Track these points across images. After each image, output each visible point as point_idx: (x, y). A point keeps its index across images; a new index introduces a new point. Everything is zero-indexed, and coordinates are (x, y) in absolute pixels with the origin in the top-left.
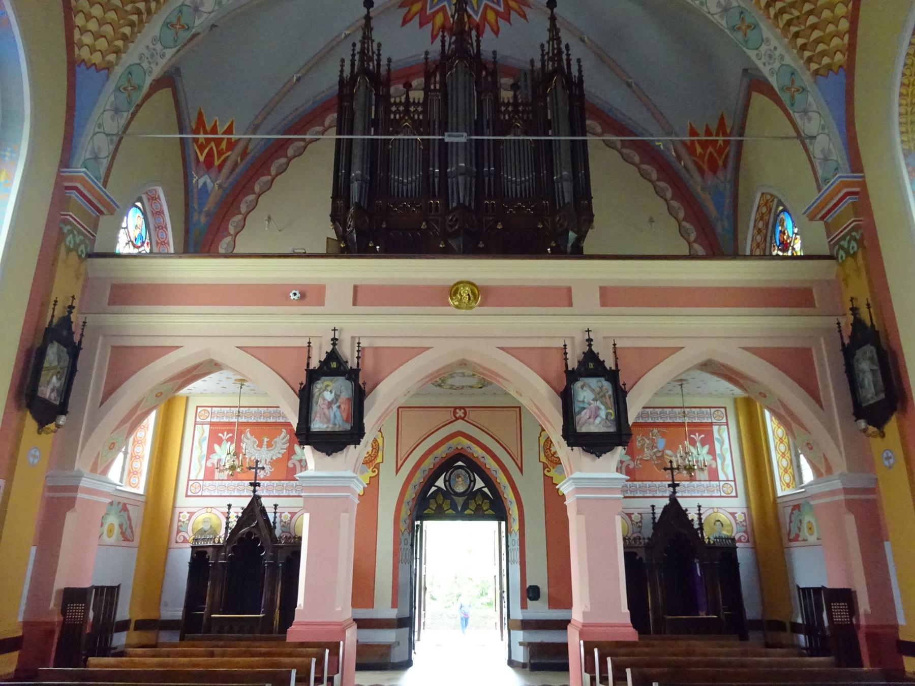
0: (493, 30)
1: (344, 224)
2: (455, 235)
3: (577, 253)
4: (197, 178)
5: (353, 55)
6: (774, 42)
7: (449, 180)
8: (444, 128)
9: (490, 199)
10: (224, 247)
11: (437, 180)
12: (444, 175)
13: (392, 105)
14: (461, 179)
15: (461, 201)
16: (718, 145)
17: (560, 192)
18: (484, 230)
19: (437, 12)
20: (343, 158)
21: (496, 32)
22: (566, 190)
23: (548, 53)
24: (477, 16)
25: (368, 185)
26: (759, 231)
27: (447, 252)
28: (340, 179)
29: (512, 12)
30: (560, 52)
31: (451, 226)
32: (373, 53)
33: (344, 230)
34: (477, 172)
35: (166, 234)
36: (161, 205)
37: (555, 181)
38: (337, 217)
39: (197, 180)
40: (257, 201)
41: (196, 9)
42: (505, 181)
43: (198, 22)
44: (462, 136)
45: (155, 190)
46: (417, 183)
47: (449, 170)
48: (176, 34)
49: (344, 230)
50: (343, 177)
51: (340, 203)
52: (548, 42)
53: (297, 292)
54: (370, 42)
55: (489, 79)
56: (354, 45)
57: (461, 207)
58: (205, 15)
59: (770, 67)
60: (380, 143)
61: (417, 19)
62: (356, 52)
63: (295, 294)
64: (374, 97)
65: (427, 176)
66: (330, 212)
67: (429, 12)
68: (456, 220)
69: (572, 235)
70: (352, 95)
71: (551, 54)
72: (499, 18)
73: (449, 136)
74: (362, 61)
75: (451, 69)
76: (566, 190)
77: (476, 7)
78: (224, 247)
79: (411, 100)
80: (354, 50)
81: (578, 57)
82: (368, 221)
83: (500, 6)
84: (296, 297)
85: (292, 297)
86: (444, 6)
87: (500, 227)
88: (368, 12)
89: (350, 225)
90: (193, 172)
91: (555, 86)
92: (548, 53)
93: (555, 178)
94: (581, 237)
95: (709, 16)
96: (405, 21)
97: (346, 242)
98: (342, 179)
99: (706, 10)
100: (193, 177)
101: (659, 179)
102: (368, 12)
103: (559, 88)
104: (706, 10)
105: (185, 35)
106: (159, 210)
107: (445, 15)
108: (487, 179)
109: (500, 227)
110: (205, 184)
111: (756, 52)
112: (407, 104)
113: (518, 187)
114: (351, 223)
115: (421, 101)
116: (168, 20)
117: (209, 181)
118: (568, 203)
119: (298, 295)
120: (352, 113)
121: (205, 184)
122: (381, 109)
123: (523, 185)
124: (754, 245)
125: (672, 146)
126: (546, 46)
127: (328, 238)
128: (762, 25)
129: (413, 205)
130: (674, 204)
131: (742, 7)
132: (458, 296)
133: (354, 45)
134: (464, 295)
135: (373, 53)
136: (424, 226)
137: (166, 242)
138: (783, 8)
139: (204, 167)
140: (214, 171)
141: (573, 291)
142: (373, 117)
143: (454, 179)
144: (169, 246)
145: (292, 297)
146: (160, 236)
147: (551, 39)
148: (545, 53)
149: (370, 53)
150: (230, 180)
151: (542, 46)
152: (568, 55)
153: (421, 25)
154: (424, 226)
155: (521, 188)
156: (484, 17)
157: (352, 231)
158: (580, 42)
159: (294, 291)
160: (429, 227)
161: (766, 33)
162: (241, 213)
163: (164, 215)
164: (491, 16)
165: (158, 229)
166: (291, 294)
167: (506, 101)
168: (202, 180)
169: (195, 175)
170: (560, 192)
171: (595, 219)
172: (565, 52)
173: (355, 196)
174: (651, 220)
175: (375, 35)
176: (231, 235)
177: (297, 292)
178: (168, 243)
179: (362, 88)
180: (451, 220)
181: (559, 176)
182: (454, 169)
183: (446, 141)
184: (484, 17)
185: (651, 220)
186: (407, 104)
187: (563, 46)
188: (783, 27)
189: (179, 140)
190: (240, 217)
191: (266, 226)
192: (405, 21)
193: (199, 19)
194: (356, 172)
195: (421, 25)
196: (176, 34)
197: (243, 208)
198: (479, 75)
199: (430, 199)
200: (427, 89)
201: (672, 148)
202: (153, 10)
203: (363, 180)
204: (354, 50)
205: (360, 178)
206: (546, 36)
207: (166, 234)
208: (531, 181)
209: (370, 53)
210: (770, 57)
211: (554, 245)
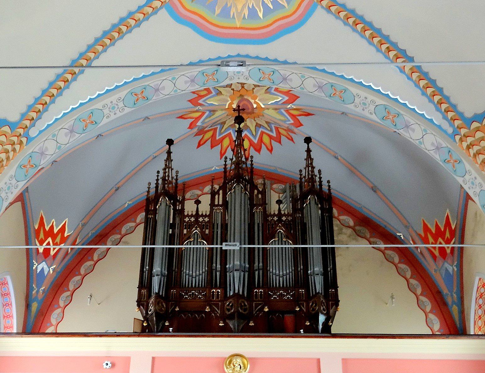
0: (268, 149)
1: (147, 309)
2: (231, 317)
3: (327, 332)
4: (37, 264)
5: (157, 180)
6: (474, 174)
7: (228, 274)
8: (224, 239)
9: (259, 288)
10: (55, 317)
11: (218, 274)
12: (224, 271)
13: (185, 217)
14: (237, 274)
15: (236, 292)
16: (446, 237)
17: (313, 281)
18: (254, 312)
19: (225, 137)
20: (147, 260)
21: (271, 150)
22: (318, 284)
23: (305, 177)
24: (255, 139)
25: (166, 277)
26: (480, 307)
27: (225, 331)
28: (144, 273)
29: (282, 137)
30: (313, 175)
31: (229, 310)
32: (172, 178)
33: (147, 313)
34: (249, 268)
35: (9, 298)
36: (8, 289)
37: (309, 274)
38: (141, 303)
39: (37, 266)
40: (82, 281)
41: (42, 154)
42: (271, 274)
43: (42, 162)
44: (236, 245)
45: (5, 278)
46: (203, 276)
47: (227, 266)
48: (27, 172)
49: (147, 313)
50: (147, 272)
51: (144, 291)
52: (305, 168)
53: (109, 363)
54: (170, 169)
55: (260, 196)
56: (158, 172)
57: (236, 296)
58: (48, 157)
59: (474, 190)
60: (175, 250)
61: (209, 143)
62: (159, 178)
63: (107, 364)
64: (172, 211)
65: (210, 271)
66: (136, 298)
67: (218, 138)
68: (232, 305)
69: (322, 318)
70: (155, 209)
71: (307, 178)
72: (272, 141)
73: (226, 245)
74: (164, 184)
75: (230, 190)
76: (318, 284)
77: (254, 133)
78: (55, 317)
79: (200, 213)
80: (158, 176)
81: (329, 179)
82: (165, 306)
83: (273, 132)
84: (108, 367)
85: (105, 366)
86: (230, 133)
87: (266, 310)
88: (170, 148)
89: (151, 309)
90: (34, 261)
91: (309, 202)
92: (305, 177)
93: (309, 272)
94: (330, 318)
95: (427, 151)
96: (199, 145)
97: (148, 322)
98: (146, 274)
99: (424, 147)
100: (33, 265)
101: (400, 262)
102: (170, 148)
103: (313, 202)
104: (424, 147)
105: (32, 171)
106: (6, 292)
107: (231, 138)
108: (257, 273)
109: (266, 310)
110: (43, 269)
111: (462, 179)
112: (197, 215)
113: (281, 279)
114: (152, 308)
115: (208, 213)
116: (21, 164)
117: (46, 267)
118: (319, 292)
119: (110, 365)
120: (155, 222)
121: (43, 269)
122: (177, 219)
123: (285, 277)
124: (476, 317)
125: (410, 238)
126: (303, 173)
127: (134, 318)
128: (464, 161)
129: (200, 293)
130: (413, 281)
131: (450, 148)
132: (232, 365)
133: (158, 172)
134: (236, 365)
135: (172, 178)
136: (208, 309)
137: (11, 315)
138: (480, 150)
139: (43, 256)
140: (50, 259)
141: (321, 361)
142: (171, 222)
143: (231, 274)
144: (13, 318)
145: (105, 366)
146: (7, 323)
147: (308, 166)
148: (302, 177)
149: (170, 179)
150: (63, 264)
151: (301, 171)
152: (320, 178)
153: (212, 147)
154: (208, 309)
155: (283, 279)
156: (261, 140)
157: (152, 314)
158: (335, 159)
159: (106, 362)
160: (213, 310)
161: (468, 167)
162: (69, 291)
163: (10, 295)
164: (266, 139)
165: (5, 306)
166: (104, 364)
167: (272, 213)
168: (41, 266)
169: (35, 263)
170: (313, 281)
171: (340, 303)
172: (318, 176)
173: (155, 288)
174: (392, 297)
175: (174, 164)
176: (61, 307)
177: (109, 363)
178: (12, 316)
179: (163, 205)
180: (228, 305)
181: (312, 271)
182: (231, 265)
183: (223, 249)
184: (261, 140)
185: (392, 297)
186: (197, 215)
187: (316, 172)
188: (481, 164)
189: (25, 249)
190: (68, 293)
191: (89, 302)
192: (199, 145)
193: (43, 160)
194: (157, 269)
195: (212, 147)
196: (27, 172)
197: (71, 287)
198: (252, 193)
199: (213, 288)
200: (212, 204)
201: (411, 239)
202: (11, 157)
203: (162, 275)
204: (158, 176)
205: (159, 273)
206: (304, 163)
207: (9, 298)
208: (291, 274)
209: (170, 179)
210: (473, 183)
211: (308, 324)
